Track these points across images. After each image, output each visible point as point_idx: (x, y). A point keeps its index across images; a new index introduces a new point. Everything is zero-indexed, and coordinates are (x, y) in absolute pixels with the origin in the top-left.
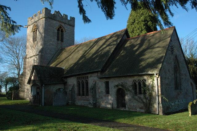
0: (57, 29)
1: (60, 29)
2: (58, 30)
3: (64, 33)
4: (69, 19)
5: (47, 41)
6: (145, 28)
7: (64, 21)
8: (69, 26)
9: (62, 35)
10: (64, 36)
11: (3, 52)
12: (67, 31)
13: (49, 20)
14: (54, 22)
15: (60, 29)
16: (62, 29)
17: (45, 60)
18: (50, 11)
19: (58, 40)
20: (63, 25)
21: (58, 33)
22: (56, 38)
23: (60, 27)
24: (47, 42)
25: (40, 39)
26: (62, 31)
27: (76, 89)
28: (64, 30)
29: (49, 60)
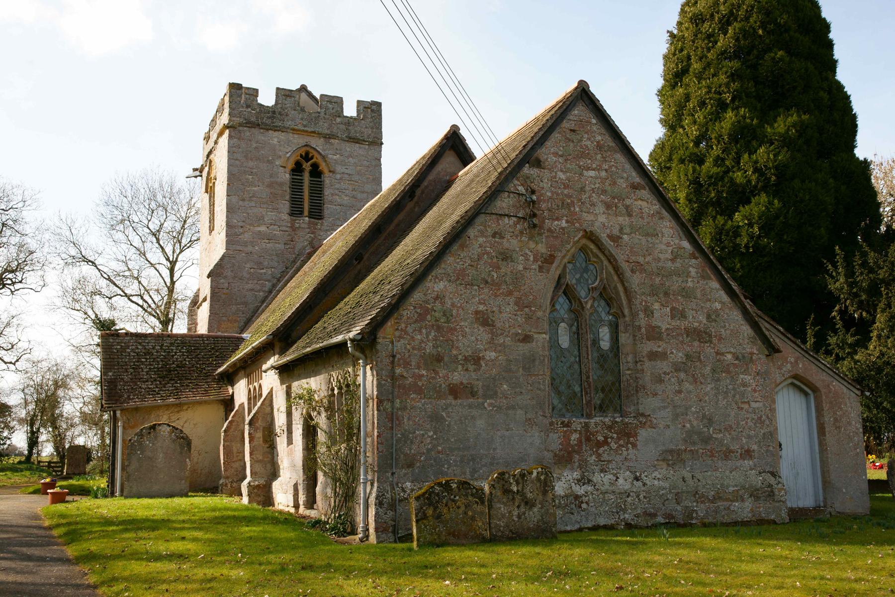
0: (291, 165)
1: (307, 166)
2: (297, 169)
3: (327, 179)
4: (350, 110)
5: (240, 224)
6: (798, 112)
7: (323, 127)
8: (349, 147)
9: (317, 191)
10: (327, 192)
11: (738, 396)
12: (339, 169)
13: (247, 133)
14: (275, 138)
15: (307, 166)
16: (315, 166)
17: (234, 308)
18: (254, 93)
19: (296, 211)
20: (318, 144)
21: (296, 187)
22: (285, 206)
23: (307, 157)
24: (241, 230)
25: (551, 549)
26: (316, 172)
27: (337, 340)
28: (323, 167)
29: (252, 307)
